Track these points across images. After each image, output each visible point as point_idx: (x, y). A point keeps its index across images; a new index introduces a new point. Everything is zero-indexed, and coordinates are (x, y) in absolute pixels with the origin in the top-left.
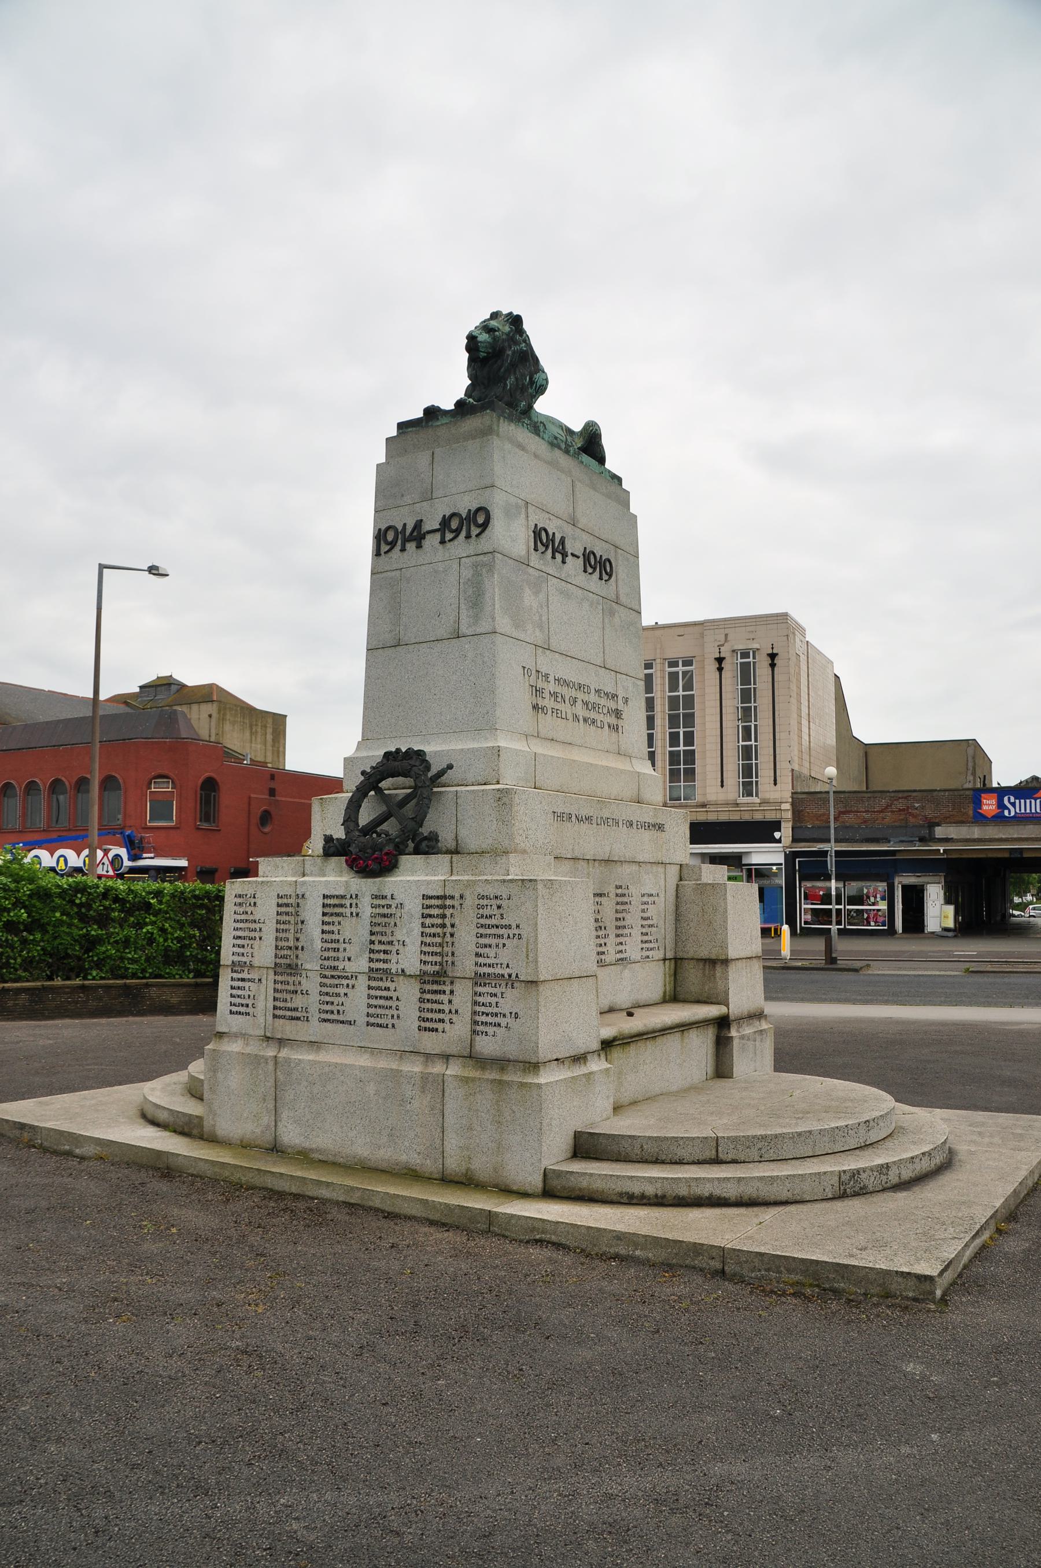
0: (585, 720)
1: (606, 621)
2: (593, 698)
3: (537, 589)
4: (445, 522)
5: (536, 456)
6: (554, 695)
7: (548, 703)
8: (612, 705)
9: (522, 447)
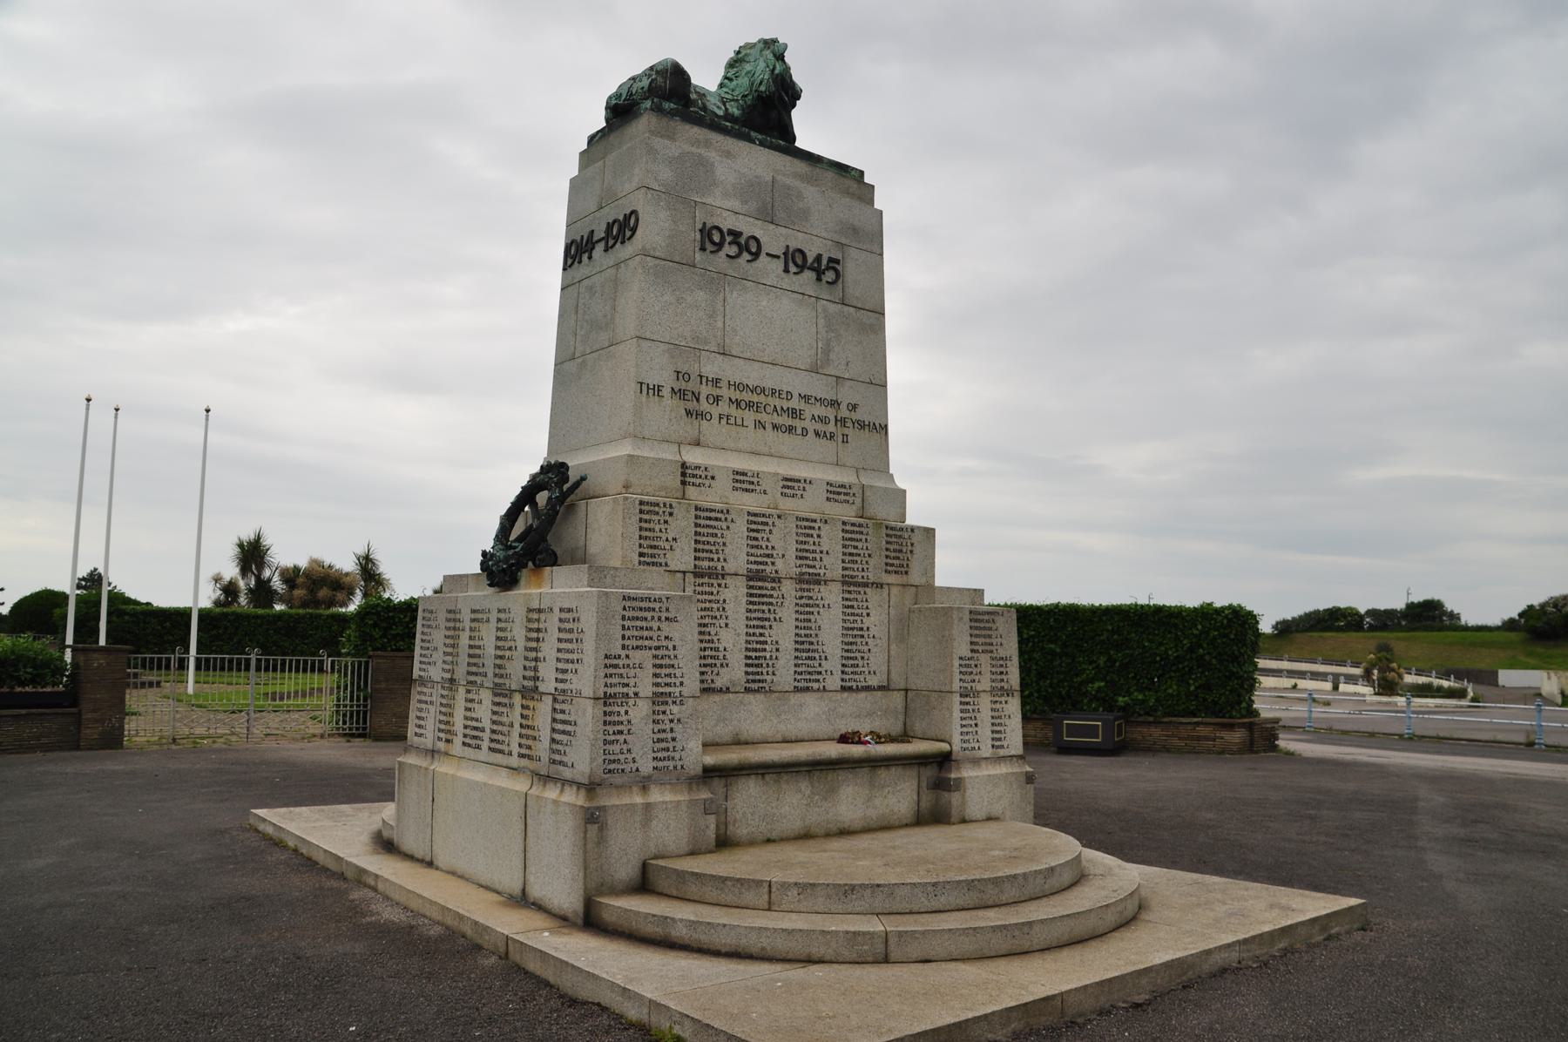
4: (610, 227)
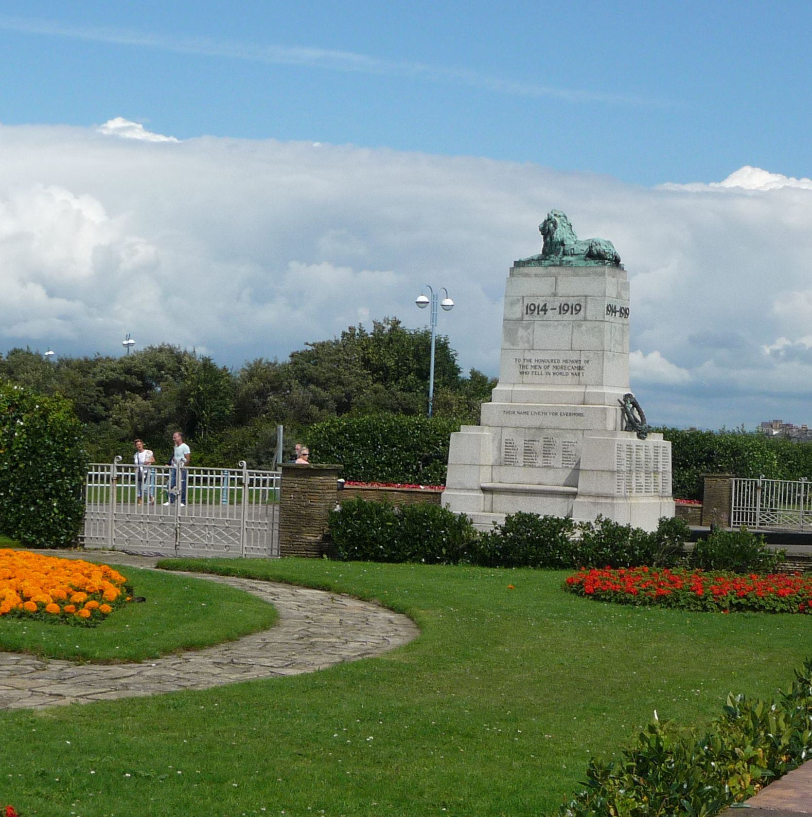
0: (554, 374)
1: (575, 330)
2: (561, 364)
3: (527, 328)
5: (536, 275)
6: (535, 367)
7: (530, 370)
8: (577, 365)
9: (527, 275)
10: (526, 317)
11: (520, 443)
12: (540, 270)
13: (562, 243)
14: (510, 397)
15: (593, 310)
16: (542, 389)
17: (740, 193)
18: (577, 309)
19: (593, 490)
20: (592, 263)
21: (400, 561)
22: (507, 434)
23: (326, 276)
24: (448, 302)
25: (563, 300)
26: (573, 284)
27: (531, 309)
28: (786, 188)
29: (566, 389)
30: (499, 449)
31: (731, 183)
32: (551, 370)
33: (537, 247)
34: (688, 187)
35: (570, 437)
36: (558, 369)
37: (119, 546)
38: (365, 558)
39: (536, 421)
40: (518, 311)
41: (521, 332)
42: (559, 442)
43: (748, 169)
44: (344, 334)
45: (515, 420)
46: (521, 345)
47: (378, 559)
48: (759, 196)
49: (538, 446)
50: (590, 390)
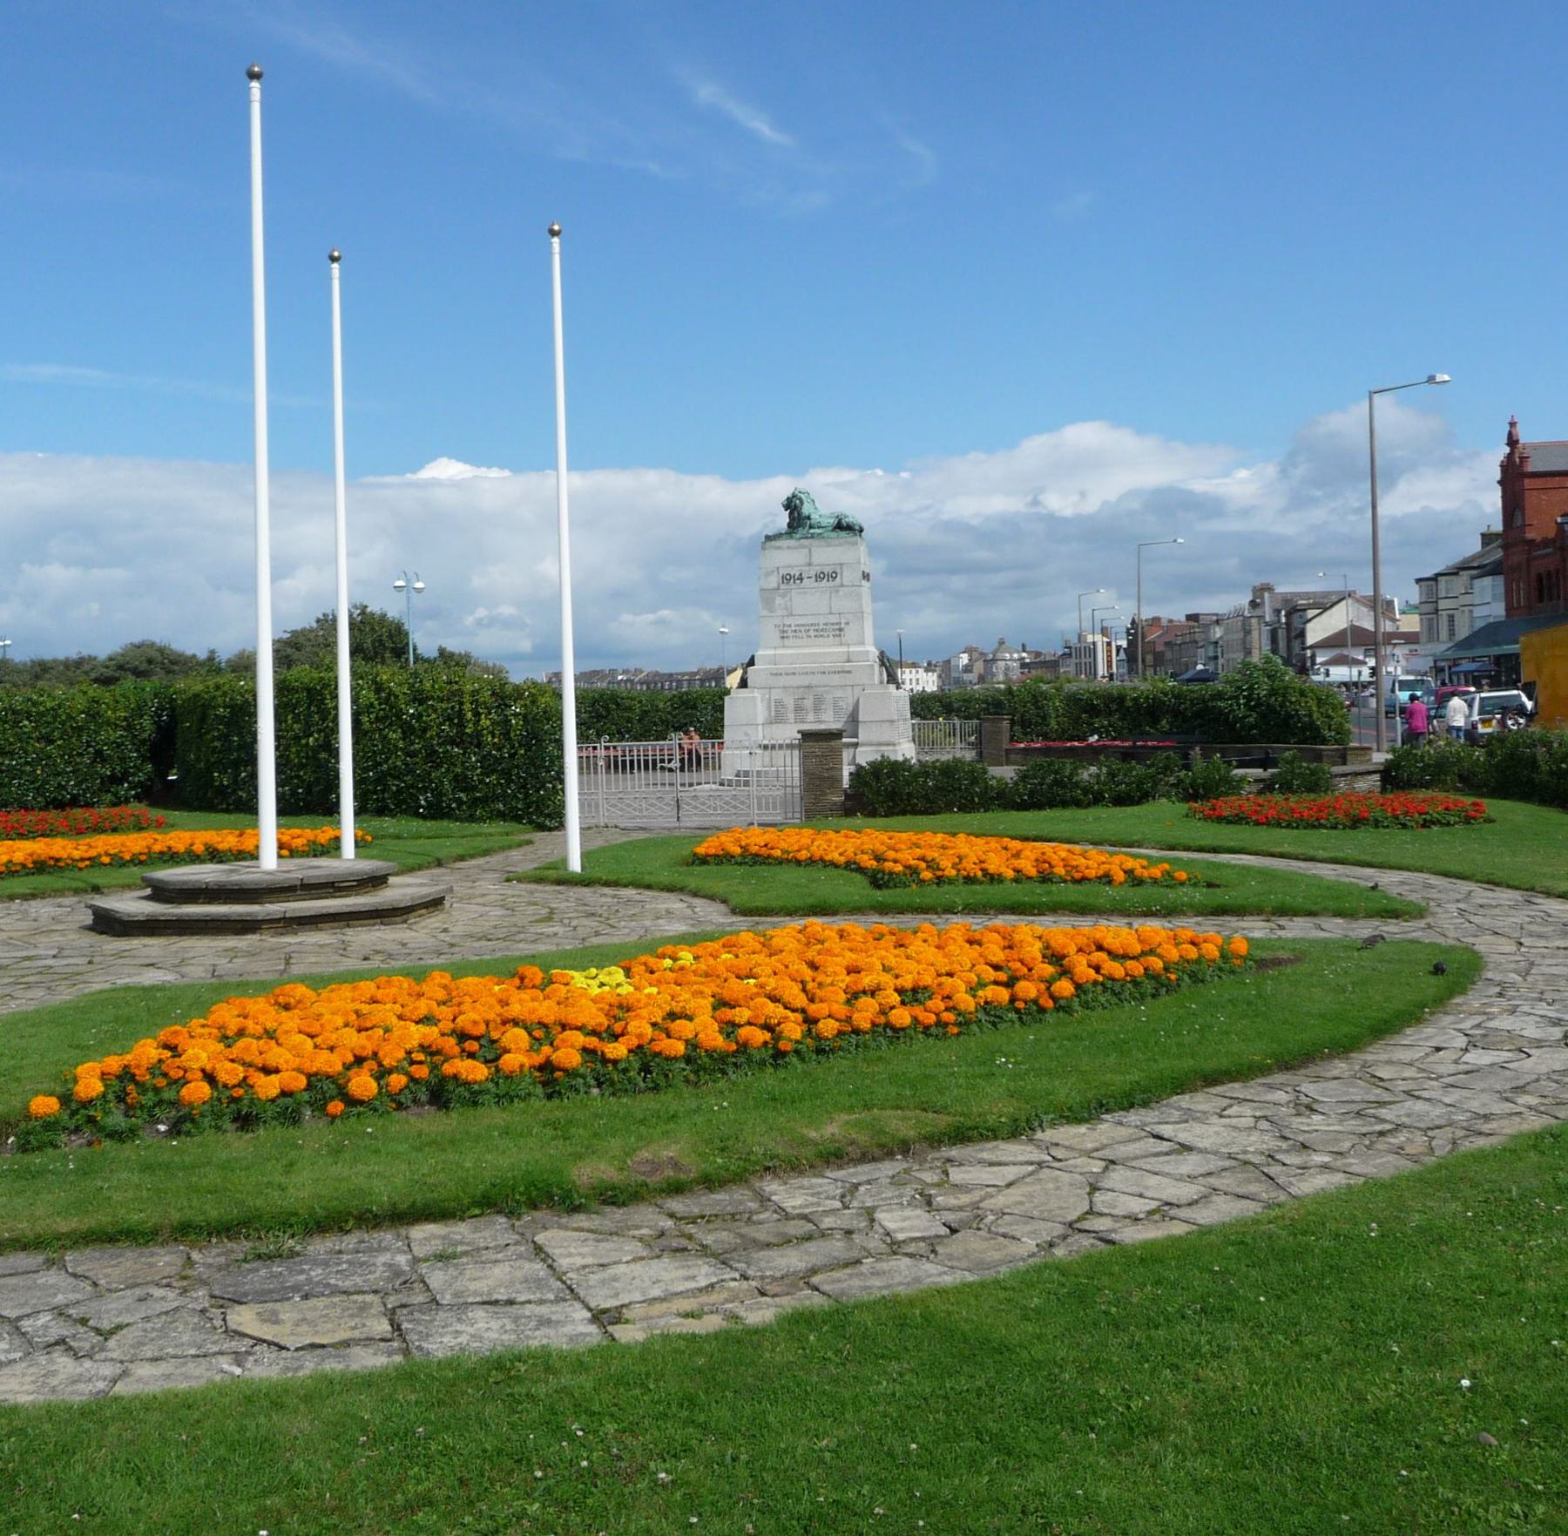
3: (783, 596)
10: (783, 587)
11: (790, 703)
12: (792, 543)
13: (809, 518)
14: (774, 660)
15: (849, 576)
16: (807, 651)
17: (435, 483)
18: (833, 576)
19: (875, 739)
20: (843, 534)
21: (933, 813)
22: (776, 694)
23: (57, 575)
24: (419, 585)
25: (819, 569)
26: (827, 553)
27: (787, 579)
28: (475, 477)
29: (828, 651)
30: (769, 708)
31: (426, 474)
32: (812, 633)
33: (783, 519)
34: (388, 479)
35: (839, 694)
36: (820, 632)
37: (611, 822)
38: (904, 813)
39: (806, 681)
40: (773, 581)
41: (779, 600)
42: (829, 698)
43: (444, 461)
44: (318, 621)
45: (783, 681)
46: (780, 612)
47: (915, 812)
48: (455, 484)
49: (809, 703)
50: (852, 649)
